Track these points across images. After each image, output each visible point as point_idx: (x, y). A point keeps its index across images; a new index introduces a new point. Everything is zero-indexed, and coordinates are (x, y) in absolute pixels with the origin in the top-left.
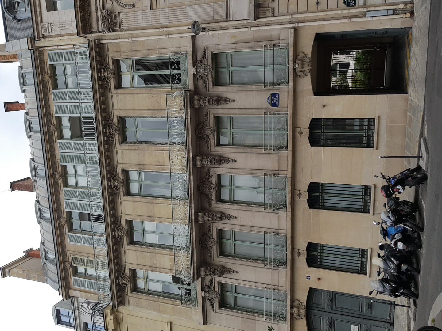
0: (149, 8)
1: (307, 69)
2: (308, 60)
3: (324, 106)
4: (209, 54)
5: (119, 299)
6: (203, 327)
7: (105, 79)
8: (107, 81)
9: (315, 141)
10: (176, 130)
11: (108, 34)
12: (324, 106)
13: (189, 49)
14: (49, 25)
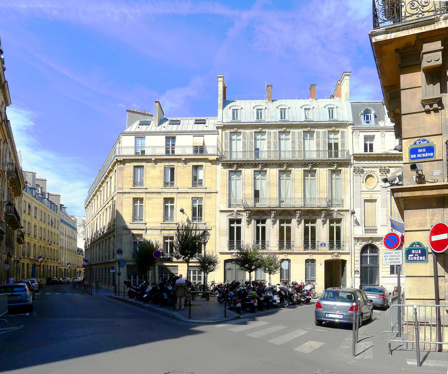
0: (361, 190)
1: (335, 258)
2: (338, 258)
3: (321, 264)
4: (342, 217)
5: (228, 165)
6: (218, 210)
7: (333, 165)
8: (332, 166)
9: (307, 261)
10: (44, 207)
11: (352, 169)
12: (321, 264)
13: (344, 209)
14: (384, 136)
